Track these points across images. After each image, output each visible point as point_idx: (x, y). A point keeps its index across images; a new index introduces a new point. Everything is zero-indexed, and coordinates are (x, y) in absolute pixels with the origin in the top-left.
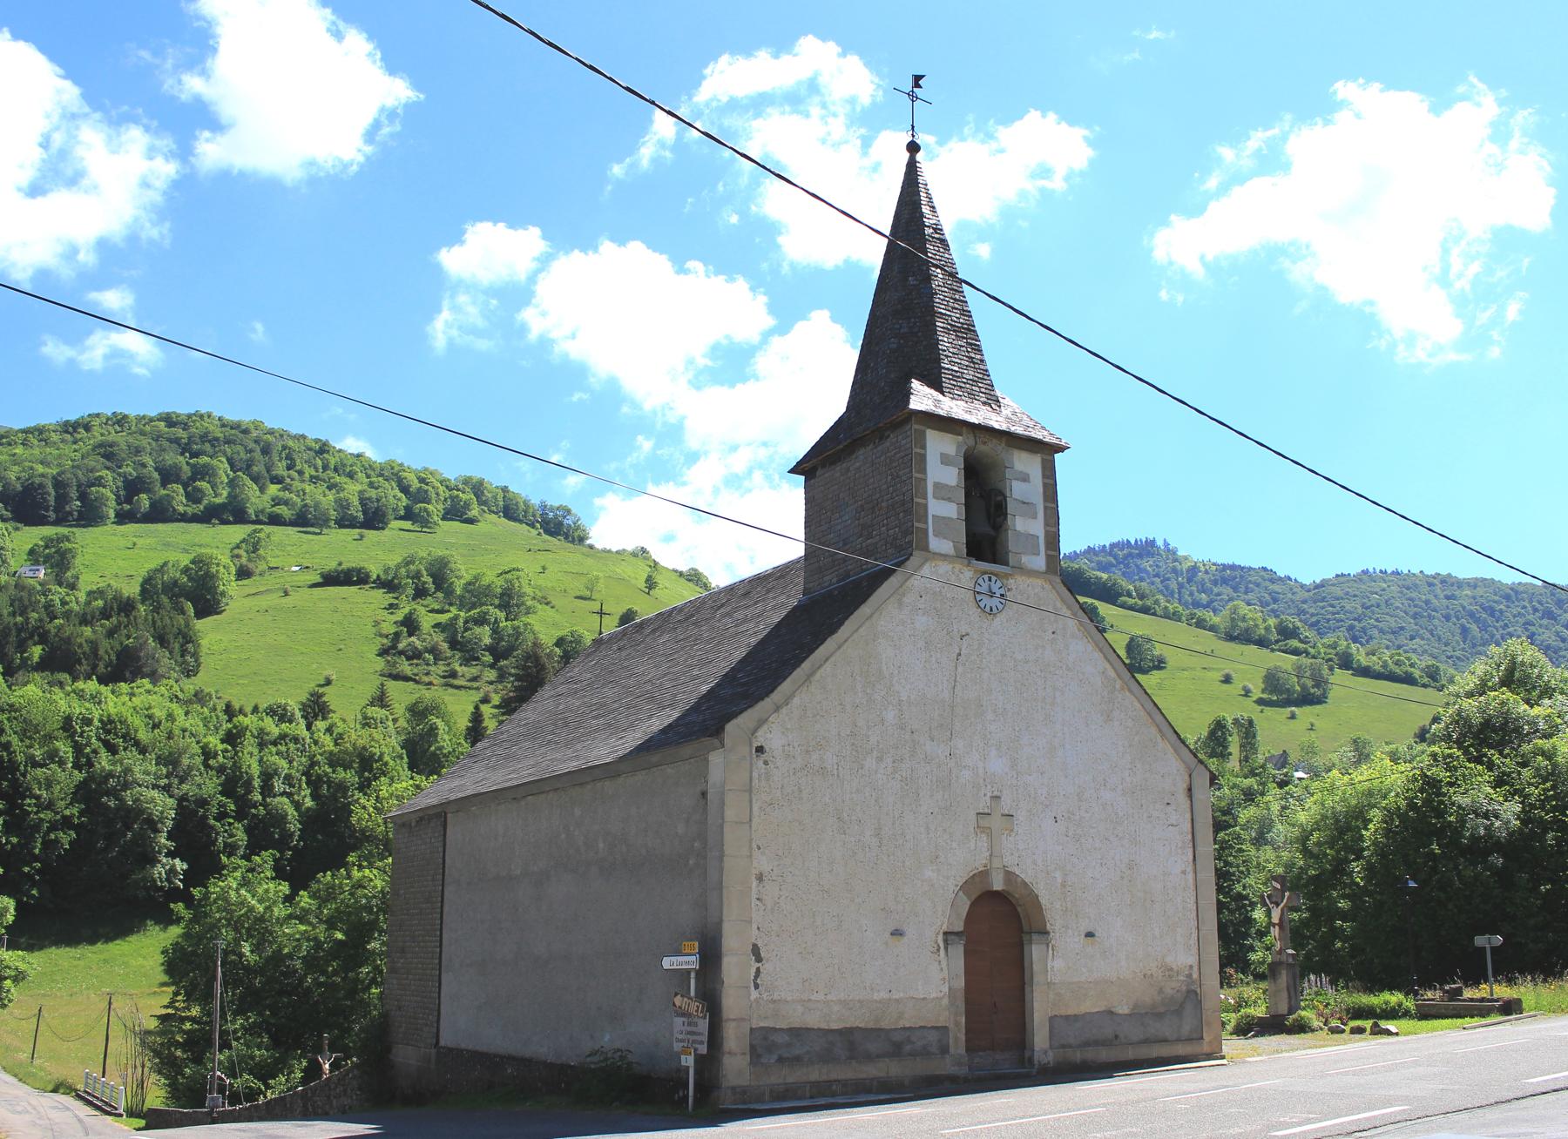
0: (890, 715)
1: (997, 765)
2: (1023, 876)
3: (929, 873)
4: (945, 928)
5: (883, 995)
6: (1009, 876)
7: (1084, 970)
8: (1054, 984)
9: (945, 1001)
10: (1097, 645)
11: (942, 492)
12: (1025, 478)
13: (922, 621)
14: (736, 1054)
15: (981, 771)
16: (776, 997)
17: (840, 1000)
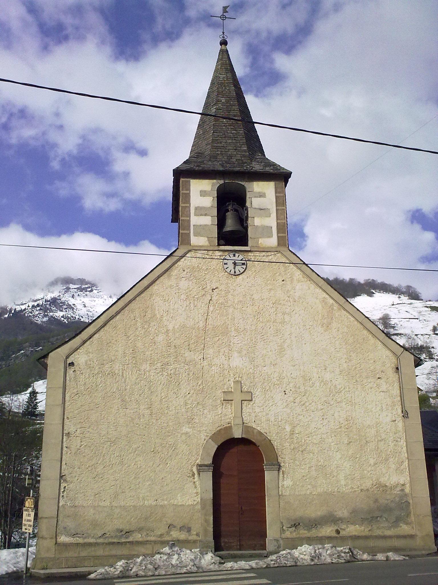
0: (160, 338)
1: (237, 361)
2: (259, 428)
3: (186, 429)
4: (198, 462)
5: (151, 502)
6: (247, 428)
7: (309, 487)
8: (283, 496)
9: (199, 507)
10: (317, 284)
11: (201, 211)
12: (262, 195)
13: (184, 284)
14: (46, 538)
15: (226, 366)
16: (77, 504)
17: (120, 506)
